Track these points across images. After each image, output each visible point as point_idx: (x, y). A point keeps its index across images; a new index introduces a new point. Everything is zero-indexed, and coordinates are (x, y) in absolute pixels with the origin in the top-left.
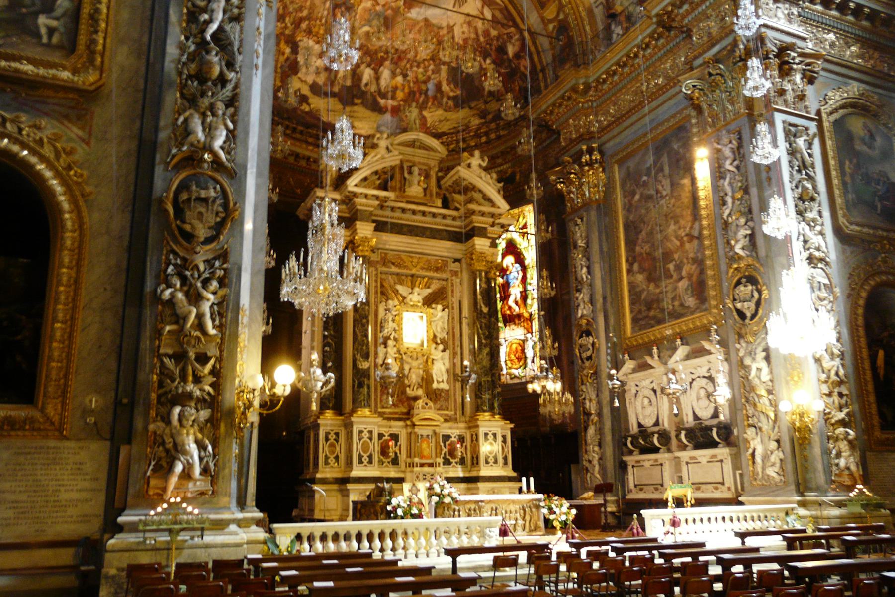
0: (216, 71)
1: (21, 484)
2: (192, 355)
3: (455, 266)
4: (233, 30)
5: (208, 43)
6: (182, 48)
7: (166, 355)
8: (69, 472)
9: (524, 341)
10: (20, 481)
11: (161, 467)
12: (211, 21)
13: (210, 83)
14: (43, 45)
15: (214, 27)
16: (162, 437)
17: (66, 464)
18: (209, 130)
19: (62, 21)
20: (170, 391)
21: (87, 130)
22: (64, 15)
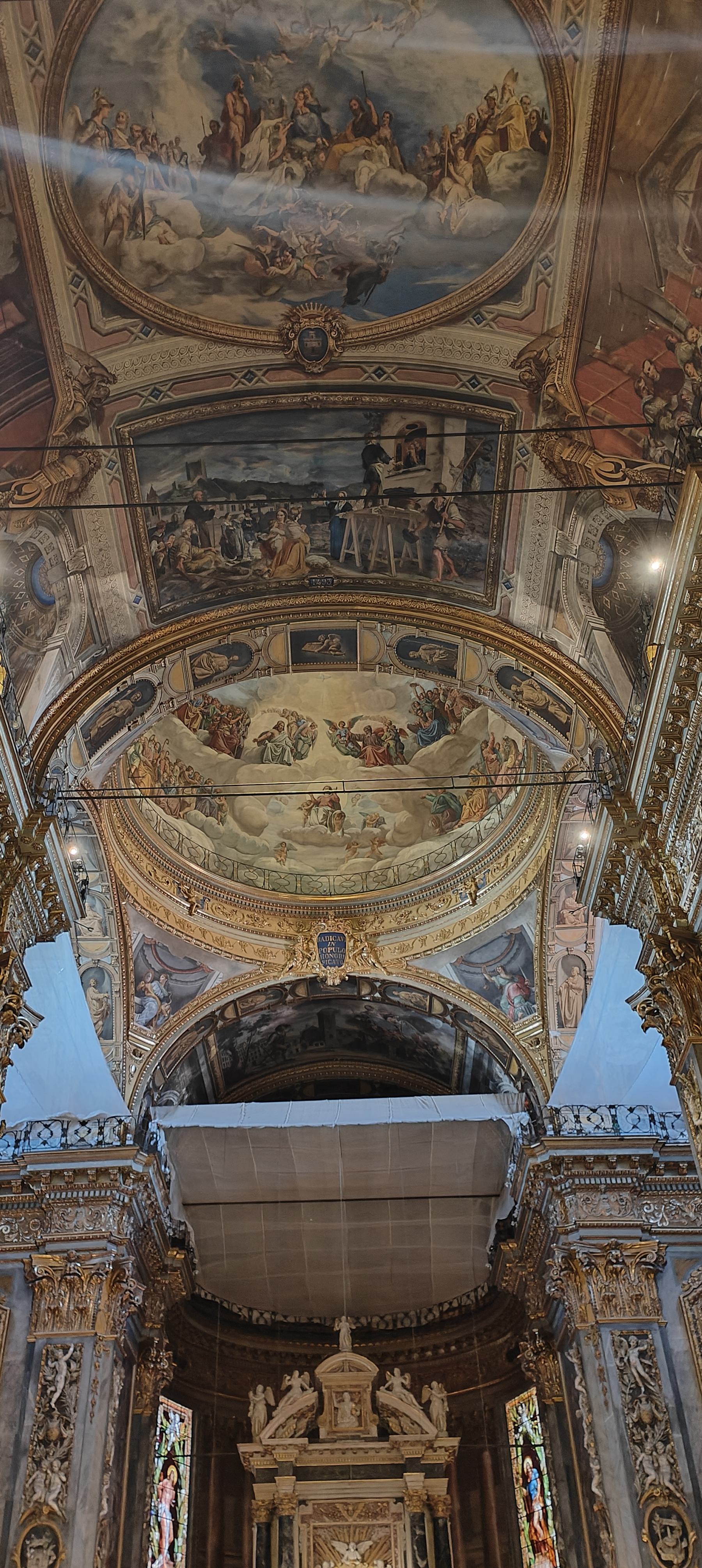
3: (395, 1508)
15: (56, 1396)
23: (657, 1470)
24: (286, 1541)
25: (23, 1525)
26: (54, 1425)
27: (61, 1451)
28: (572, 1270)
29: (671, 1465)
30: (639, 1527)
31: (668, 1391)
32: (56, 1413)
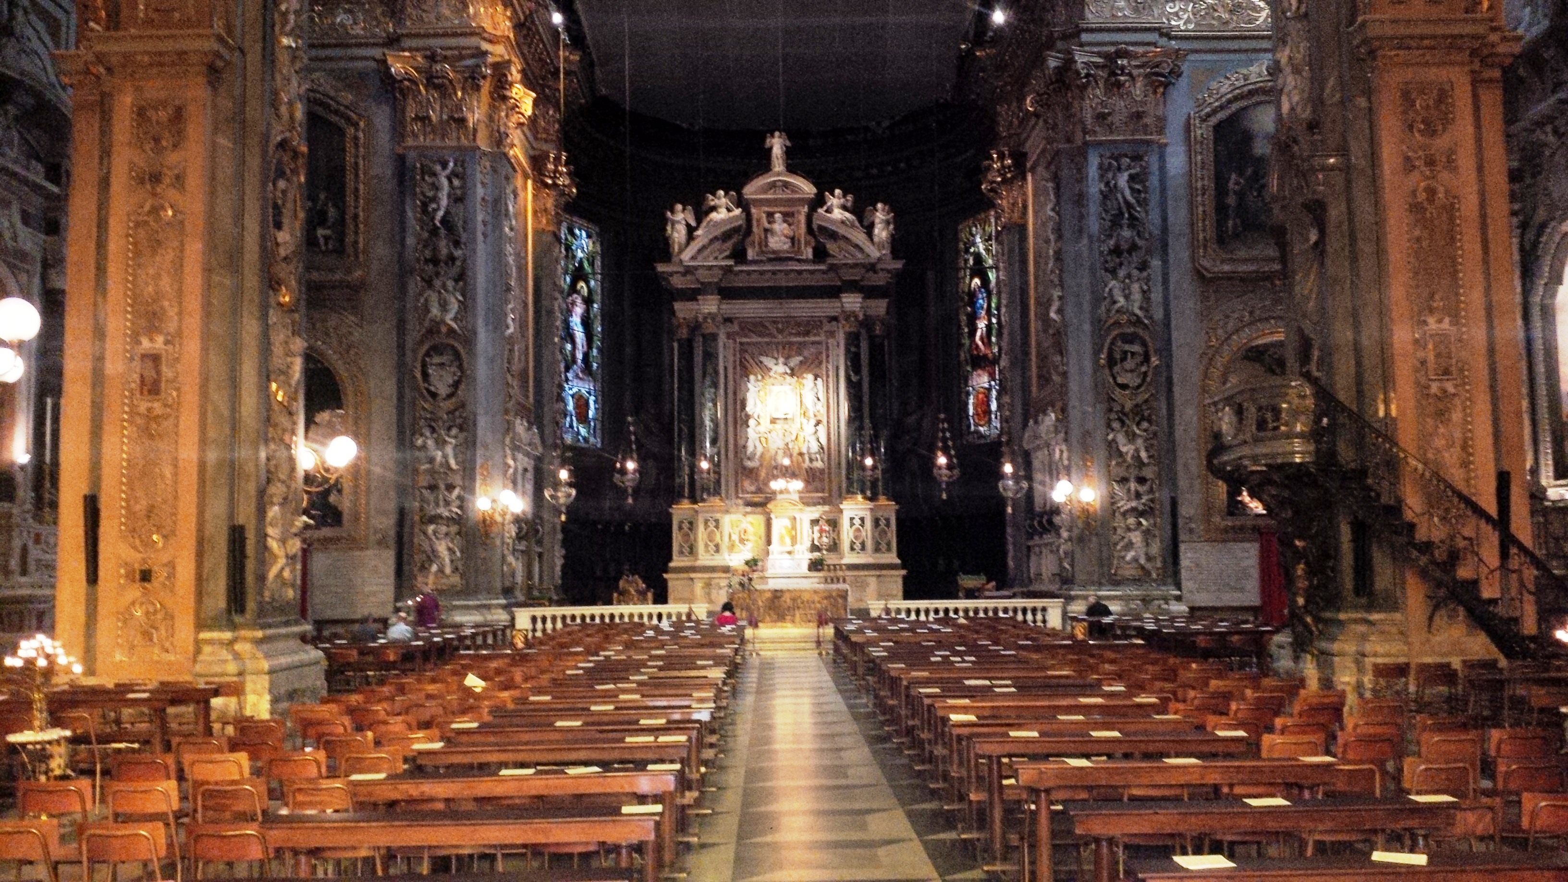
2: (442, 486)
6: (418, 236)
9: (989, 390)
12: (438, 209)
15: (441, 213)
18: (444, 306)
23: (1127, 297)
24: (710, 356)
25: (421, 342)
26: (444, 247)
27: (455, 271)
28: (1064, 82)
29: (1144, 292)
30: (1096, 353)
31: (1154, 217)
32: (443, 232)
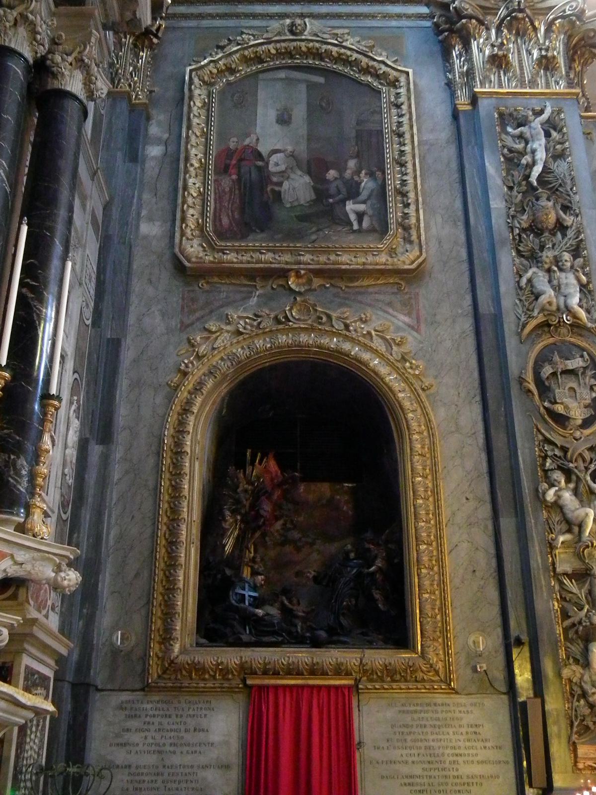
0: (552, 218)
1: (413, 752)
4: (560, 168)
5: (535, 189)
7: (565, 574)
8: (465, 737)
10: (411, 748)
11: (587, 728)
12: (534, 163)
13: (546, 234)
14: (354, 231)
15: (537, 170)
16: (581, 687)
17: (460, 726)
19: (369, 202)
20: (580, 623)
21: (414, 316)
22: (369, 197)
